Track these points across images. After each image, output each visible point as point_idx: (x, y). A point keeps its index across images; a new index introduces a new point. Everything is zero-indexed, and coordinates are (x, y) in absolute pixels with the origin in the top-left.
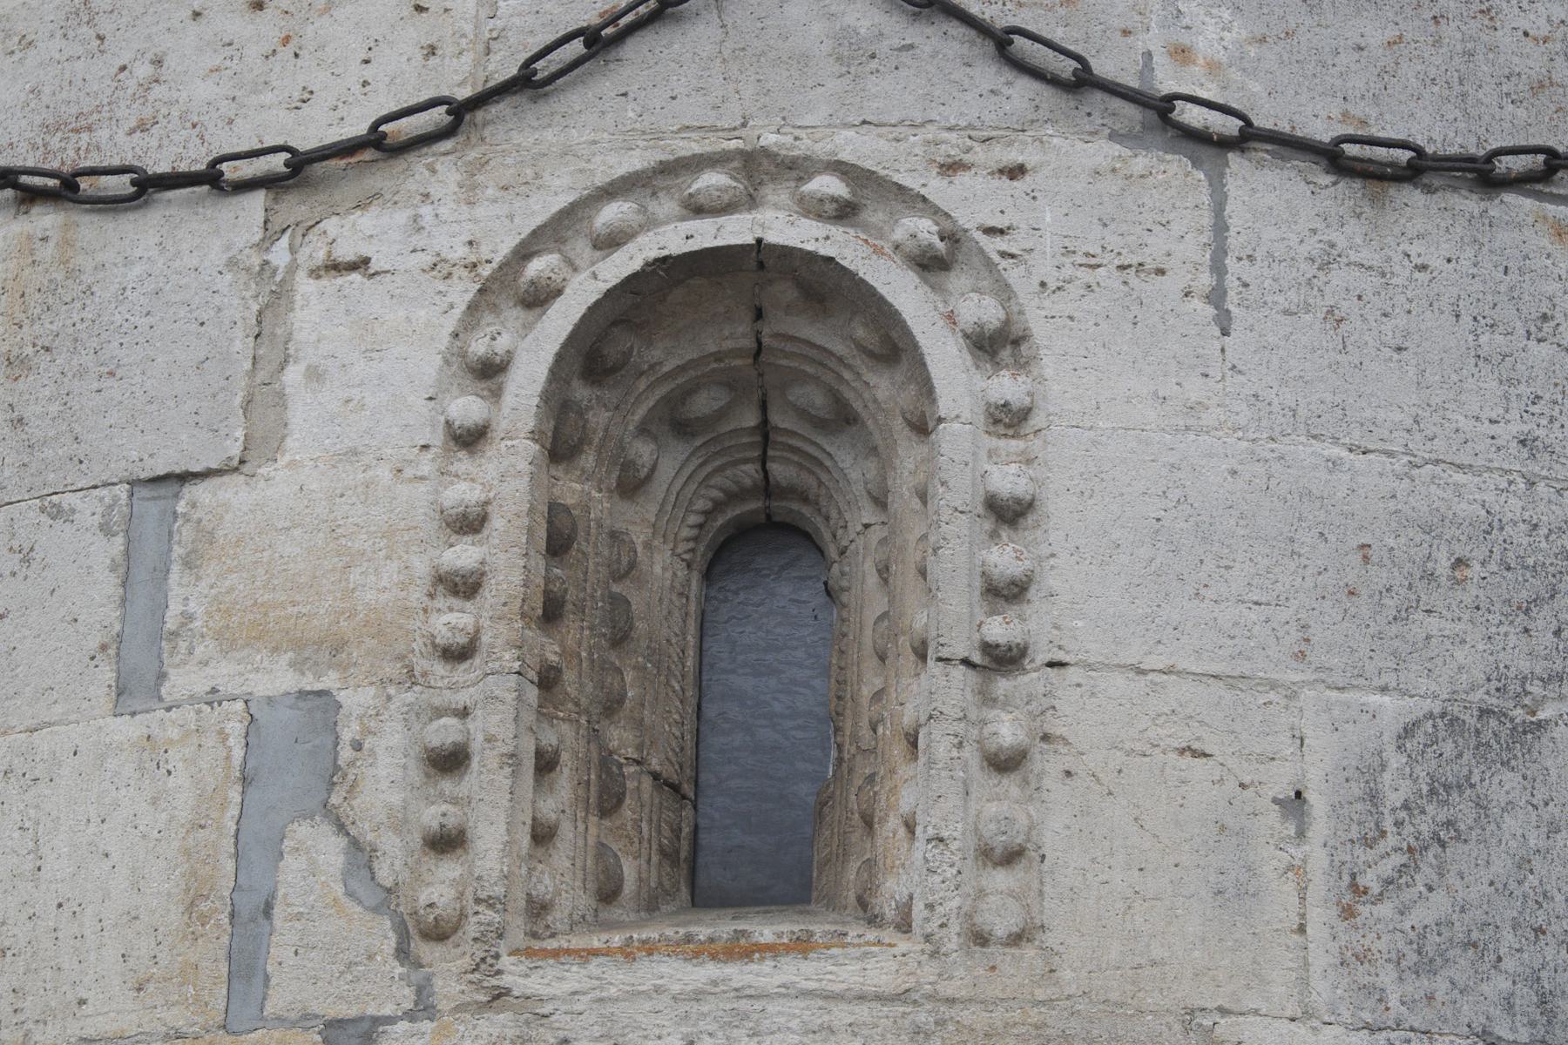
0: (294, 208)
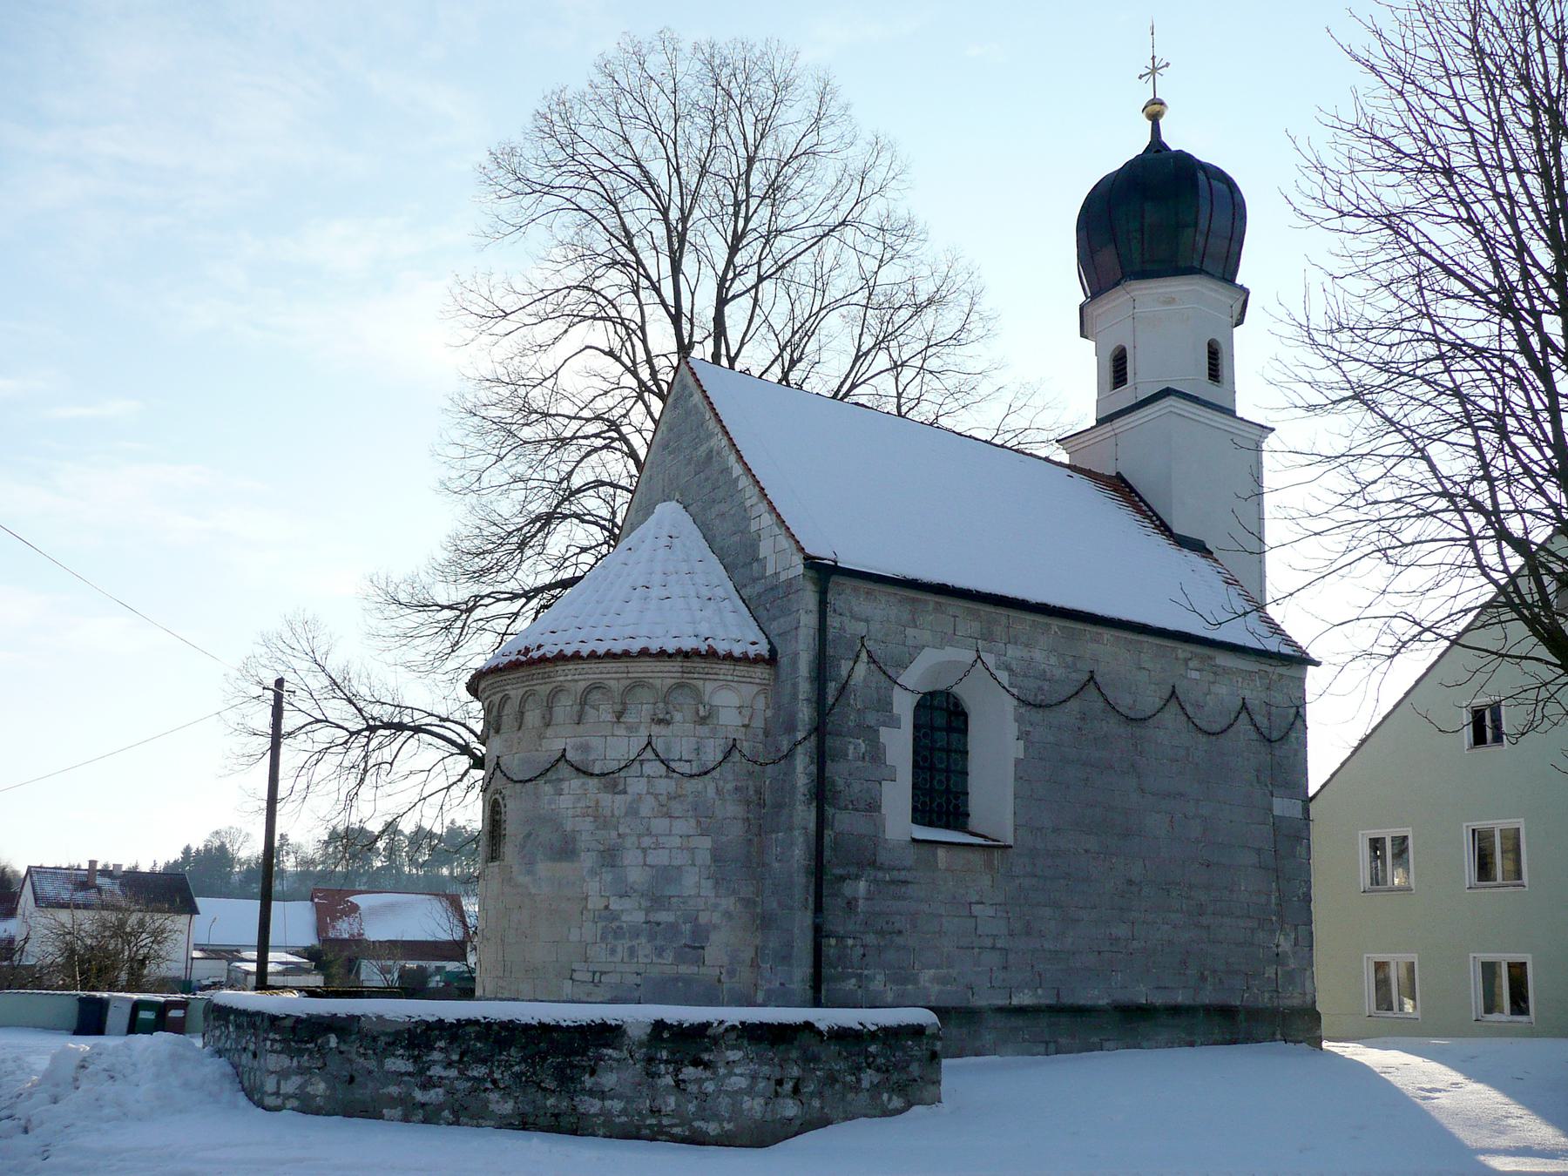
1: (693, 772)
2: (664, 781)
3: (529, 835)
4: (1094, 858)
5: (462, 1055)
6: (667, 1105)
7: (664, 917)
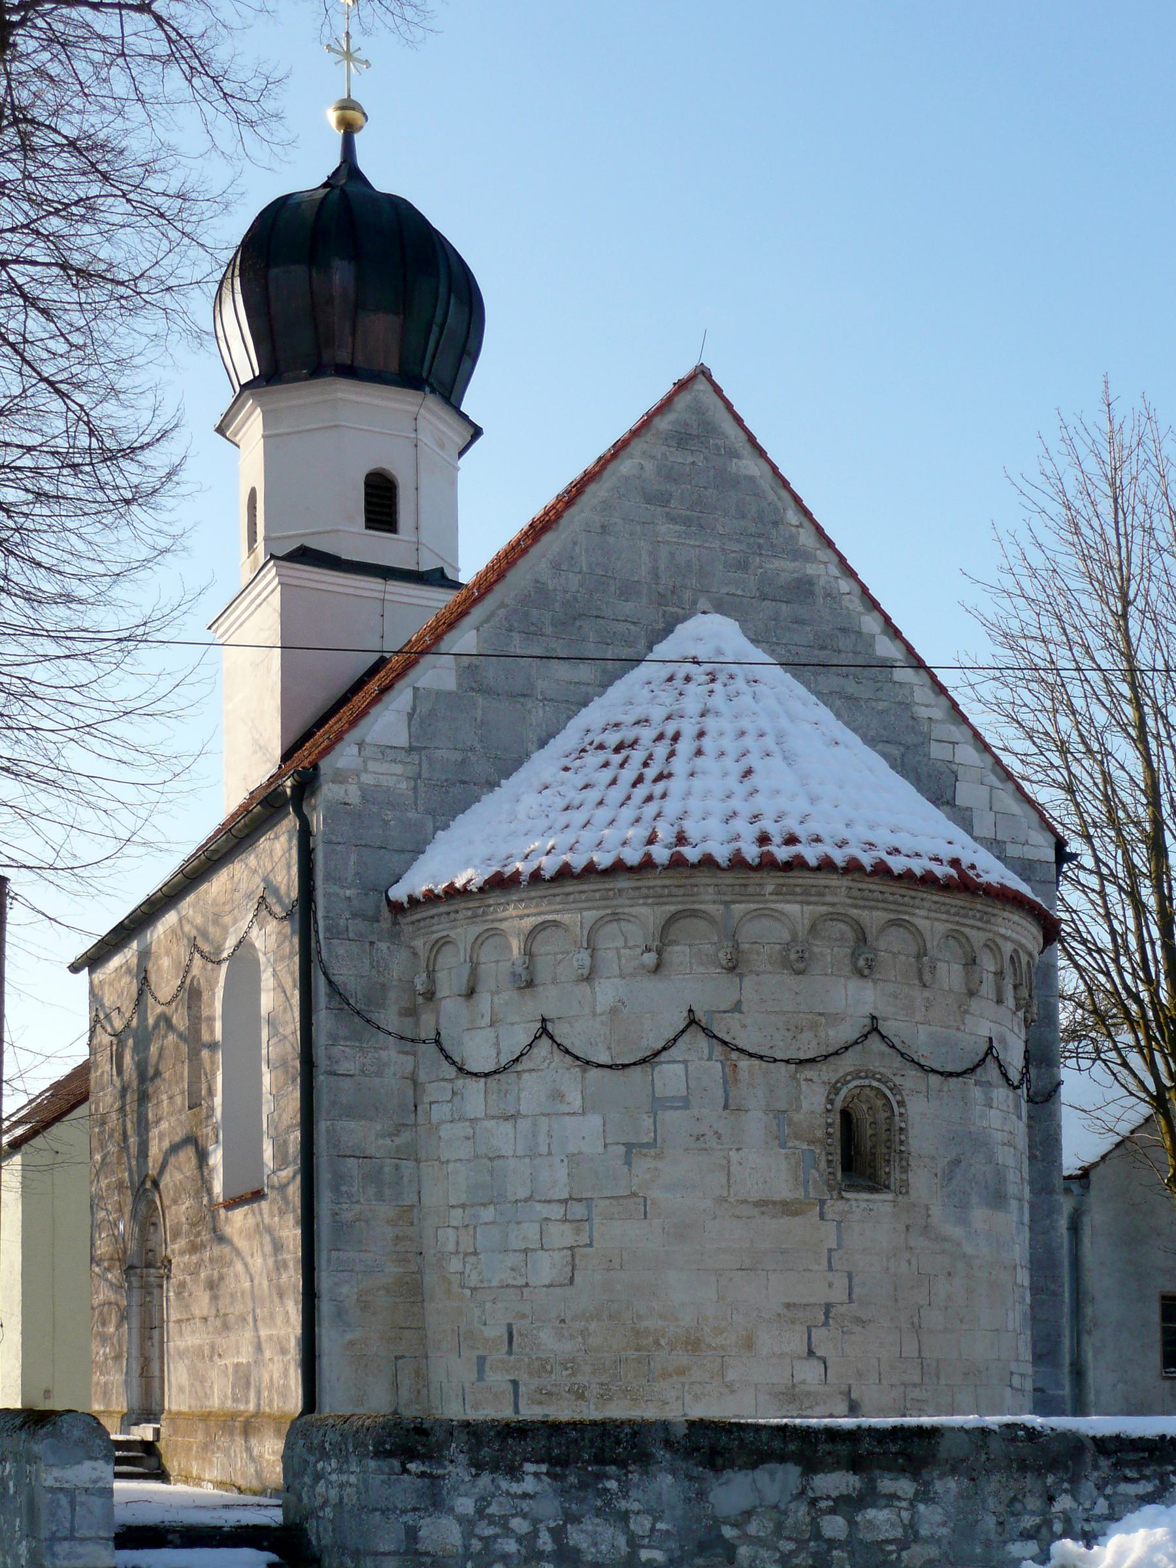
0: (800, 1068)
3: (956, 1162)
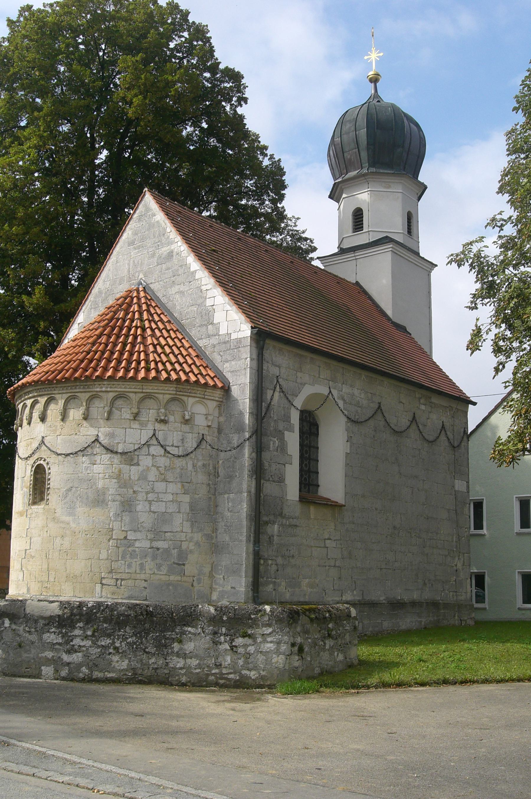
1: (180, 454)
2: (163, 459)
4: (379, 513)
5: (94, 632)
6: (225, 661)
7: (161, 544)
